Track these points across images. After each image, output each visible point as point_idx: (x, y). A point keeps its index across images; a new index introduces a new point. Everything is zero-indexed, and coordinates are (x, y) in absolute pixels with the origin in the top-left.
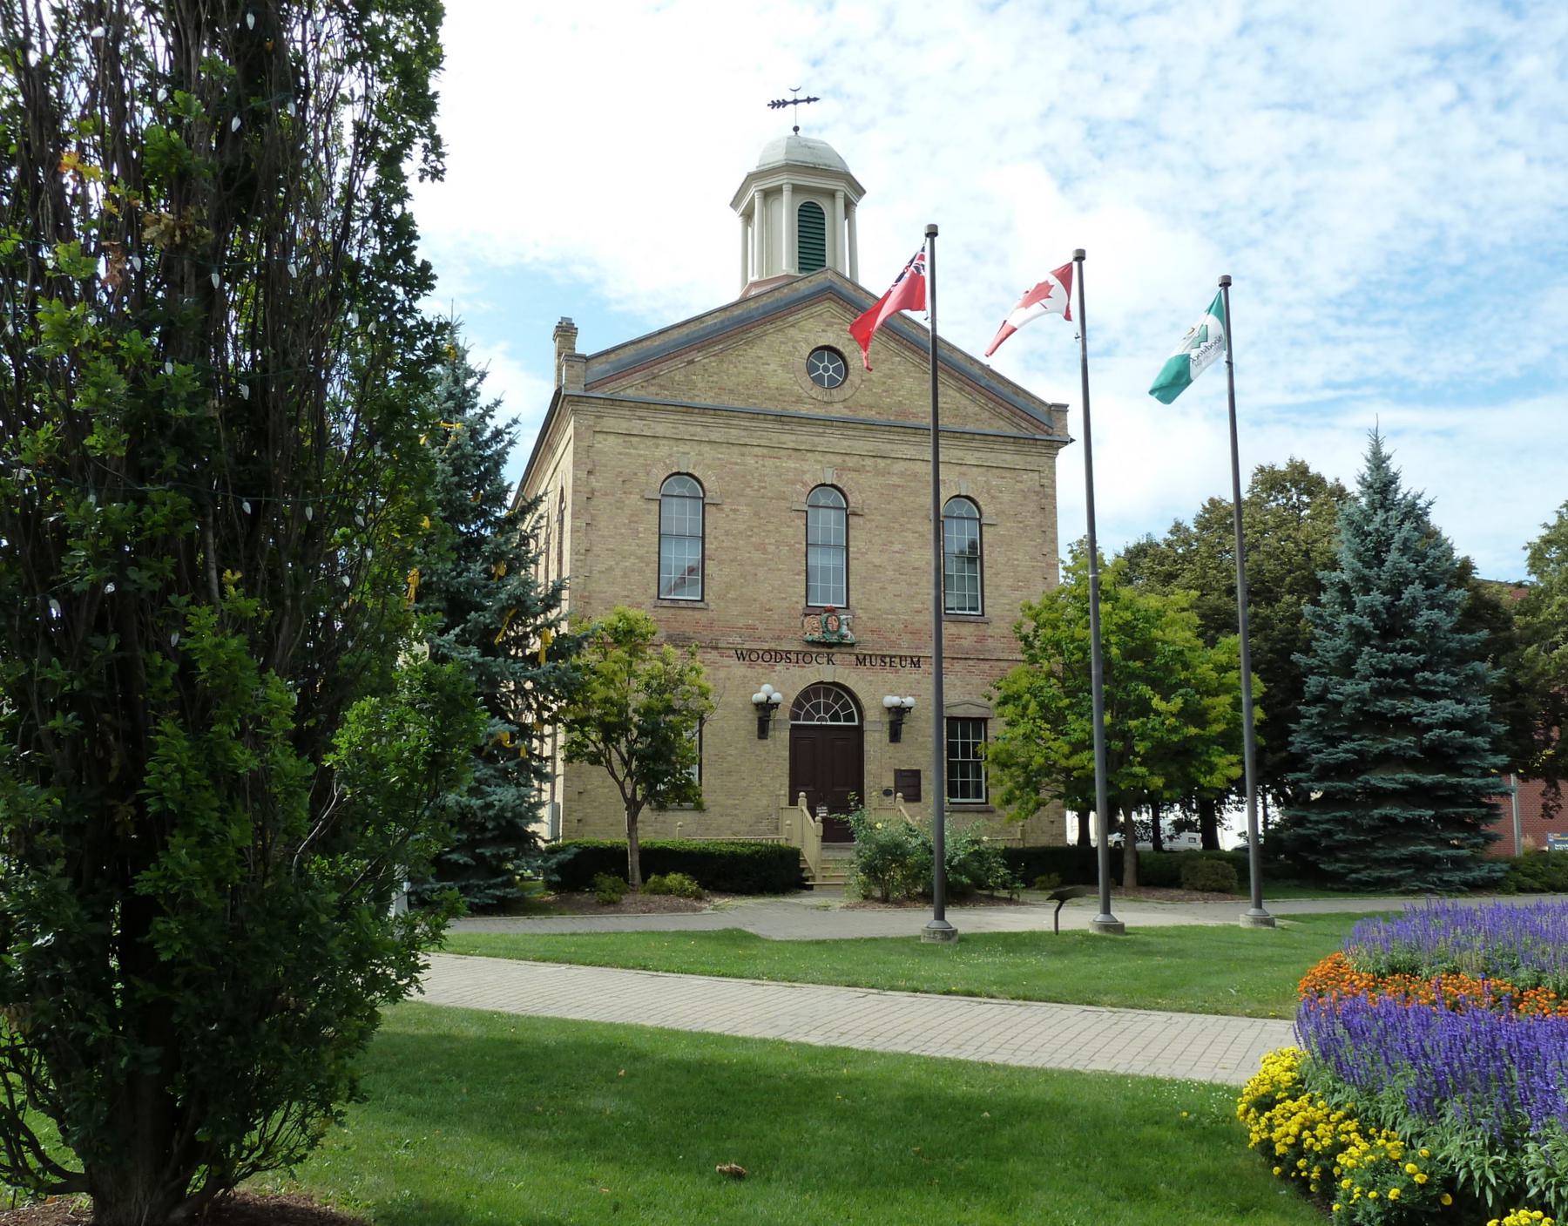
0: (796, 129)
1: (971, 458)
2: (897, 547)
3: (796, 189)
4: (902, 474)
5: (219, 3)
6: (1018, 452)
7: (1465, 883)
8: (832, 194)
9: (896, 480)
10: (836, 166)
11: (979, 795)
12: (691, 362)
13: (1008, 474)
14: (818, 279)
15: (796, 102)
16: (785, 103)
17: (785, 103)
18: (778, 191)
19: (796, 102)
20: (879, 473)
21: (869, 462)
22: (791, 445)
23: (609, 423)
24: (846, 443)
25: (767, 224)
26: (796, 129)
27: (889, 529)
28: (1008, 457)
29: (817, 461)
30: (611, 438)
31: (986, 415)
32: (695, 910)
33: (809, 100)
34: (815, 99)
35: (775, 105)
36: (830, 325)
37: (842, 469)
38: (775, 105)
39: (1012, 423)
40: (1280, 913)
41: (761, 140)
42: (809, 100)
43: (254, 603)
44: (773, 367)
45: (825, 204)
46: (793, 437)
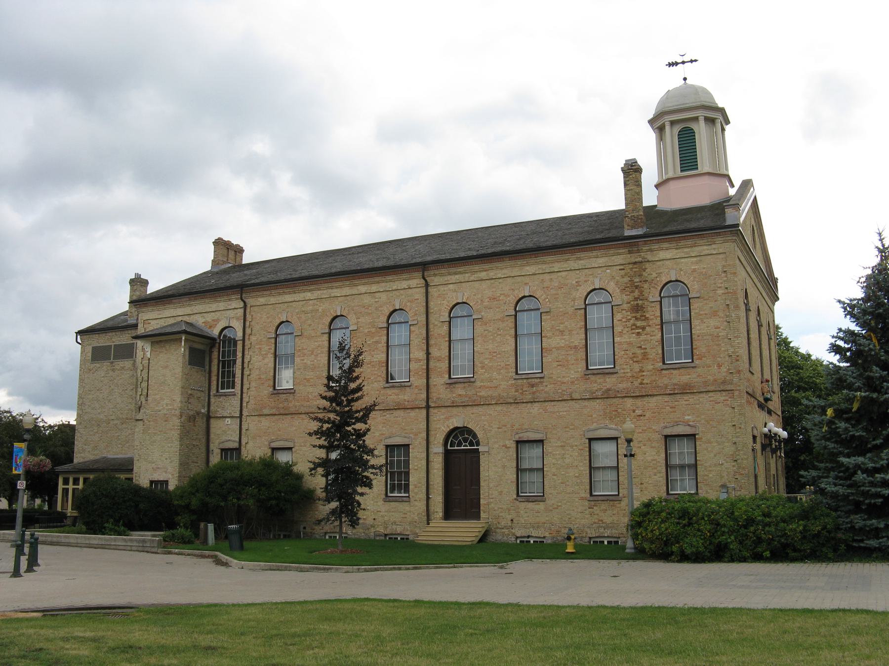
0: (685, 79)
5: (886, 472)
7: (879, 549)
8: (696, 119)
10: (705, 101)
11: (233, 388)
14: (693, 194)
15: (683, 63)
16: (676, 64)
17: (676, 64)
19: (683, 63)
26: (685, 79)
32: (219, 562)
33: (692, 61)
34: (696, 61)
35: (671, 65)
38: (671, 65)
41: (657, 86)
42: (692, 61)
45: (693, 126)
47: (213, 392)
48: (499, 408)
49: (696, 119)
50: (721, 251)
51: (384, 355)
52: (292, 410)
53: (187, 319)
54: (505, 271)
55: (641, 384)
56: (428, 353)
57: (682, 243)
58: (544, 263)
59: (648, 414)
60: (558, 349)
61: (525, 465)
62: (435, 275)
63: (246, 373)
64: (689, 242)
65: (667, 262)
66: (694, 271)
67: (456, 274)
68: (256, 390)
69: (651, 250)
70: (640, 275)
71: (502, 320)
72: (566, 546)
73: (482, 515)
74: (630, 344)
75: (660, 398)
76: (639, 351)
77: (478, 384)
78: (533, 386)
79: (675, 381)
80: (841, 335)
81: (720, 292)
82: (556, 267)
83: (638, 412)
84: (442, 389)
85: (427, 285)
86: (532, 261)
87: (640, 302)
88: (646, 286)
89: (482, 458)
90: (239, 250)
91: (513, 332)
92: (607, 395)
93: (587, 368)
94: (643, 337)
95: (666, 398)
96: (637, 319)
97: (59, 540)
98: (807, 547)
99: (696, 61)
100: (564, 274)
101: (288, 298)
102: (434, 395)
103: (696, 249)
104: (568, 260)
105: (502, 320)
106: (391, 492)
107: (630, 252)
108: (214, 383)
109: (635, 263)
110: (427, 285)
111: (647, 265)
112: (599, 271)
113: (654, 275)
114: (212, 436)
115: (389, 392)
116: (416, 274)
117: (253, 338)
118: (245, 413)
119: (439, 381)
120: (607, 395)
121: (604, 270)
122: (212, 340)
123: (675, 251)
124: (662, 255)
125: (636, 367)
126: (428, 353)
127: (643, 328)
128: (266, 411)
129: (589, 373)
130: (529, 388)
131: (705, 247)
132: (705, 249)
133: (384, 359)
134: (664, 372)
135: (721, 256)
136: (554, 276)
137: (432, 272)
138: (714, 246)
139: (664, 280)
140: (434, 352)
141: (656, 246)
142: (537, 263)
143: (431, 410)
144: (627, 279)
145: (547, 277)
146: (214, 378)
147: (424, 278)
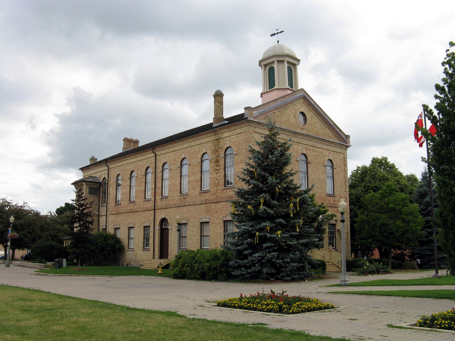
0: (278, 42)
1: (331, 149)
2: (318, 173)
3: (288, 62)
4: (318, 152)
6: (340, 148)
8: (273, 62)
9: (317, 153)
10: (286, 52)
12: (274, 113)
13: (338, 154)
15: (278, 33)
16: (274, 34)
17: (274, 34)
18: (283, 61)
19: (278, 33)
20: (314, 151)
21: (311, 147)
22: (296, 141)
23: (258, 130)
24: (307, 141)
25: (265, 69)
26: (278, 42)
27: (316, 168)
28: (338, 149)
29: (301, 147)
30: (257, 134)
31: (334, 136)
33: (281, 32)
34: (283, 31)
36: (302, 106)
37: (306, 149)
39: (339, 139)
40: (176, 245)
42: (281, 32)
43: (298, 191)
44: (291, 116)
46: (296, 139)
47: (100, 205)
48: (175, 209)
49: (273, 62)
50: (244, 131)
51: (144, 187)
52: (120, 212)
53: (93, 175)
54: (178, 147)
55: (217, 196)
56: (155, 186)
57: (232, 128)
58: (189, 142)
59: (219, 211)
60: (192, 181)
61: (205, 234)
62: (158, 151)
63: (108, 197)
64: (233, 128)
65: (227, 138)
66: (236, 141)
67: (164, 150)
68: (111, 203)
69: (221, 133)
70: (218, 145)
71: (176, 169)
72: (158, 271)
73: (169, 257)
74: (214, 178)
75: (222, 203)
76: (217, 181)
77: (169, 198)
78: (184, 199)
79: (228, 195)
80: (246, 172)
81: (244, 151)
82: (193, 144)
83: (216, 210)
84: (159, 200)
85: (156, 156)
86: (185, 142)
87: (218, 158)
88: (220, 150)
89: (170, 231)
90: (137, 142)
91: (179, 175)
92: (206, 202)
93: (201, 190)
94: (218, 174)
95: (225, 203)
96: (217, 166)
97: (26, 265)
98: (211, 274)
99: (283, 31)
100: (195, 147)
101: (119, 164)
102: (157, 204)
103: (236, 131)
104: (196, 140)
105: (176, 169)
106: (146, 247)
107: (215, 135)
108: (101, 201)
109: (217, 140)
110: (156, 156)
111: (221, 140)
112: (205, 144)
113: (223, 145)
114: (100, 224)
115: (145, 203)
116: (150, 152)
117: (111, 182)
118: (108, 214)
119: (158, 197)
120: (206, 202)
121: (205, 143)
122: (100, 183)
123: (229, 133)
124: (226, 135)
125: (216, 188)
126: (155, 186)
127: (218, 170)
128: (113, 213)
129: (202, 192)
130: (184, 200)
131: (239, 130)
132: (239, 131)
133: (144, 189)
134: (225, 191)
135: (245, 133)
136: (192, 148)
137: (157, 150)
138: (242, 129)
139: (226, 147)
140: (157, 184)
141: (222, 131)
142: (187, 143)
143: (156, 211)
144: (214, 147)
145: (190, 148)
146: (101, 199)
147: (153, 153)
